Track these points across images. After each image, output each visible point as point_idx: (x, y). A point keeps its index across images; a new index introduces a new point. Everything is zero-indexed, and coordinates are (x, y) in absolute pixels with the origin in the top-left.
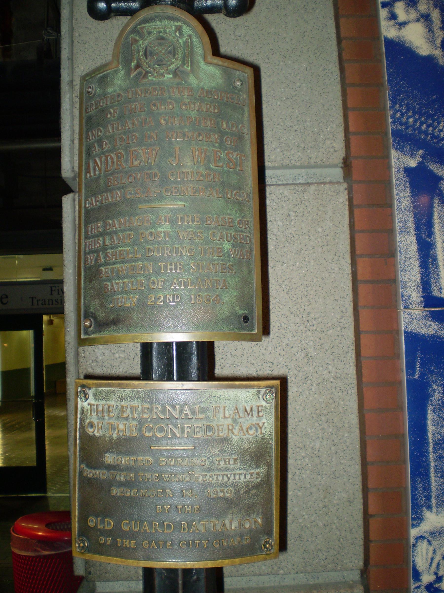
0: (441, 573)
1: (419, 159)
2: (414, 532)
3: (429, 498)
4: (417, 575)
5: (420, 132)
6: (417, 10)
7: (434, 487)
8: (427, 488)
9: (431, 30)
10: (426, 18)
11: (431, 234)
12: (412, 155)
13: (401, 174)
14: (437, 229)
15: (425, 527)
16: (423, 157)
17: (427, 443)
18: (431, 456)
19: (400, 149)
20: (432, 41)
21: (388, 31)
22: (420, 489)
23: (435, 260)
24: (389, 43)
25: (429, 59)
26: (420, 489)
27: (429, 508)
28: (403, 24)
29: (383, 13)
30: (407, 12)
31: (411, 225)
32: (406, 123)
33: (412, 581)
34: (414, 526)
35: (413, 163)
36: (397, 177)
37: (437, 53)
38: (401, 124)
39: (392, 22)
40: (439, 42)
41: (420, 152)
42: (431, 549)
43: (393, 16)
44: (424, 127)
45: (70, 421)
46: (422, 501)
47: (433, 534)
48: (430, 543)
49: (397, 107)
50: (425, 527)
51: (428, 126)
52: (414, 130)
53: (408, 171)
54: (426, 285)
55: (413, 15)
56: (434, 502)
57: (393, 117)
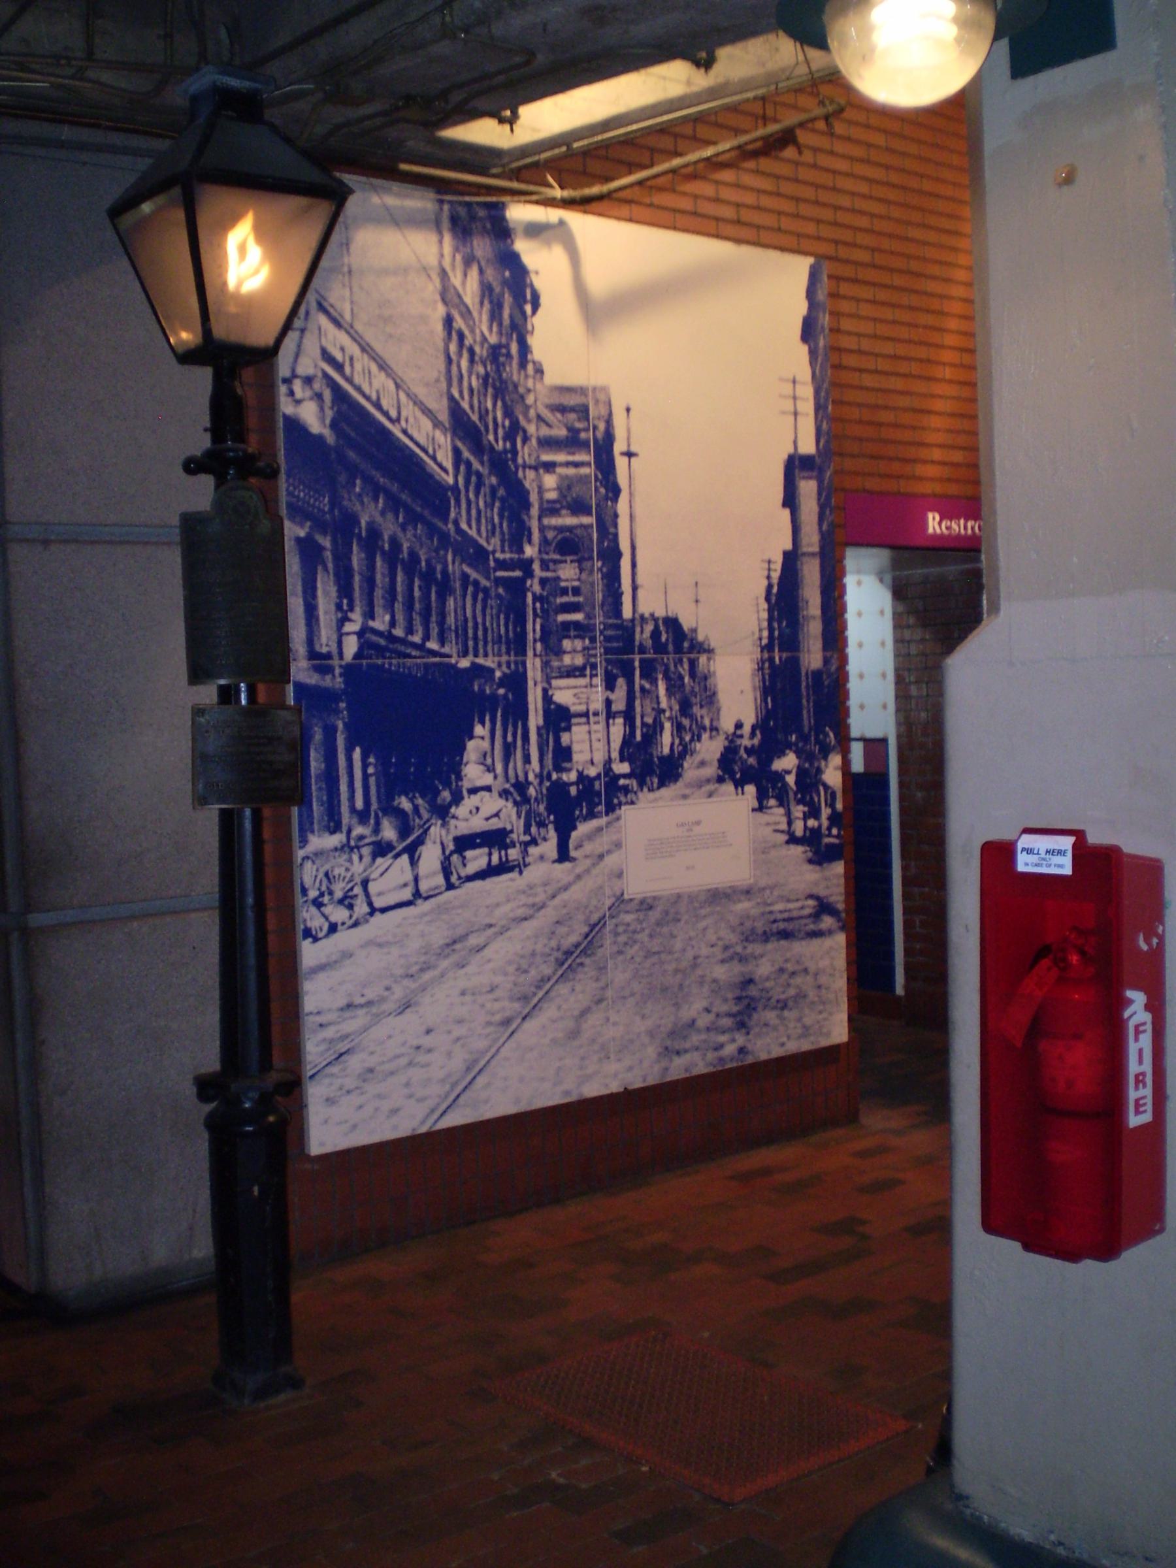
0: (1031, 780)
1: (307, 530)
2: (301, 853)
3: (312, 823)
4: (304, 891)
5: (308, 503)
6: (311, 388)
7: (315, 814)
8: (311, 816)
9: (322, 409)
10: (319, 397)
11: (314, 597)
12: (302, 526)
13: (293, 542)
14: (320, 593)
15: (310, 848)
16: (311, 527)
17: (310, 776)
18: (314, 787)
19: (292, 518)
20: (322, 419)
21: (286, 407)
22: (305, 815)
23: (318, 620)
24: (287, 418)
25: (320, 438)
26: (305, 815)
27: (313, 832)
28: (298, 402)
29: (283, 389)
30: (303, 389)
31: (299, 588)
32: (298, 497)
33: (300, 896)
34: (301, 848)
35: (302, 534)
36: (289, 545)
37: (327, 433)
38: (294, 496)
39: (290, 399)
40: (328, 422)
41: (308, 524)
42: (315, 867)
43: (291, 393)
44: (312, 501)
45: (1003, 1525)
46: (307, 826)
47: (316, 854)
48: (313, 862)
49: (291, 480)
50: (310, 848)
51: (316, 500)
52: (304, 502)
53: (298, 540)
54: (310, 642)
55: (308, 393)
56: (316, 826)
57: (287, 490)
